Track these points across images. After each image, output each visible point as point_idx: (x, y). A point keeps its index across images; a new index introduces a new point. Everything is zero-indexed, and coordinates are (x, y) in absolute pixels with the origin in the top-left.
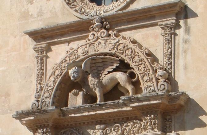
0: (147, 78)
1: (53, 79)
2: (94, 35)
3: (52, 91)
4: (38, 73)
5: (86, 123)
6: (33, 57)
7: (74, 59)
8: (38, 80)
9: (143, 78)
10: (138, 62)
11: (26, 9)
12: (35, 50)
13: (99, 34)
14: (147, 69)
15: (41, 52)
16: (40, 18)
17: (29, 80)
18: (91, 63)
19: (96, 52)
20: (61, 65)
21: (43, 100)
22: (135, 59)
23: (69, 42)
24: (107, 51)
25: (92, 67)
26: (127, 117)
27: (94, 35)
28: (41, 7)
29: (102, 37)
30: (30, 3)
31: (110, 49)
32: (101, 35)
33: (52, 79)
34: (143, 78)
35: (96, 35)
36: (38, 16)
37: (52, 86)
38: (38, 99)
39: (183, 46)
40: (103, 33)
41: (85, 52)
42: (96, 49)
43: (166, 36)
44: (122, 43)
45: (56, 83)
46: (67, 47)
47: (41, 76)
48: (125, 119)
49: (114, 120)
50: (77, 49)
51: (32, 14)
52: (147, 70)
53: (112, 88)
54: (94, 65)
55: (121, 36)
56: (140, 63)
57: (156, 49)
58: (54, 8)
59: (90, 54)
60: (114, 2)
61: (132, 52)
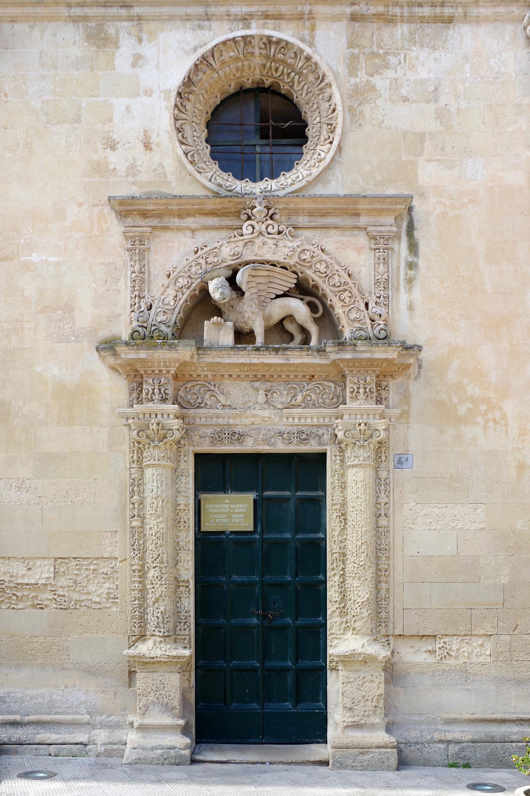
0: (355, 316)
2: (254, 228)
5: (234, 376)
6: (121, 248)
9: (348, 315)
10: (338, 287)
11: (103, 157)
12: (128, 234)
14: (356, 300)
15: (140, 241)
16: (133, 179)
19: (259, 258)
20: (189, 270)
21: (154, 328)
24: (279, 257)
26: (313, 374)
28: (134, 159)
29: (269, 234)
30: (110, 147)
32: (267, 228)
33: (171, 292)
34: (348, 315)
35: (257, 227)
36: (127, 176)
40: (270, 227)
41: (236, 253)
43: (379, 252)
44: (308, 250)
45: (180, 300)
46: (190, 240)
47: (140, 283)
48: (307, 377)
49: (288, 376)
50: (221, 246)
51: (115, 168)
52: (354, 301)
53: (275, 323)
54: (253, 279)
55: (303, 238)
56: (341, 288)
58: (161, 165)
60: (268, 179)
61: (327, 267)
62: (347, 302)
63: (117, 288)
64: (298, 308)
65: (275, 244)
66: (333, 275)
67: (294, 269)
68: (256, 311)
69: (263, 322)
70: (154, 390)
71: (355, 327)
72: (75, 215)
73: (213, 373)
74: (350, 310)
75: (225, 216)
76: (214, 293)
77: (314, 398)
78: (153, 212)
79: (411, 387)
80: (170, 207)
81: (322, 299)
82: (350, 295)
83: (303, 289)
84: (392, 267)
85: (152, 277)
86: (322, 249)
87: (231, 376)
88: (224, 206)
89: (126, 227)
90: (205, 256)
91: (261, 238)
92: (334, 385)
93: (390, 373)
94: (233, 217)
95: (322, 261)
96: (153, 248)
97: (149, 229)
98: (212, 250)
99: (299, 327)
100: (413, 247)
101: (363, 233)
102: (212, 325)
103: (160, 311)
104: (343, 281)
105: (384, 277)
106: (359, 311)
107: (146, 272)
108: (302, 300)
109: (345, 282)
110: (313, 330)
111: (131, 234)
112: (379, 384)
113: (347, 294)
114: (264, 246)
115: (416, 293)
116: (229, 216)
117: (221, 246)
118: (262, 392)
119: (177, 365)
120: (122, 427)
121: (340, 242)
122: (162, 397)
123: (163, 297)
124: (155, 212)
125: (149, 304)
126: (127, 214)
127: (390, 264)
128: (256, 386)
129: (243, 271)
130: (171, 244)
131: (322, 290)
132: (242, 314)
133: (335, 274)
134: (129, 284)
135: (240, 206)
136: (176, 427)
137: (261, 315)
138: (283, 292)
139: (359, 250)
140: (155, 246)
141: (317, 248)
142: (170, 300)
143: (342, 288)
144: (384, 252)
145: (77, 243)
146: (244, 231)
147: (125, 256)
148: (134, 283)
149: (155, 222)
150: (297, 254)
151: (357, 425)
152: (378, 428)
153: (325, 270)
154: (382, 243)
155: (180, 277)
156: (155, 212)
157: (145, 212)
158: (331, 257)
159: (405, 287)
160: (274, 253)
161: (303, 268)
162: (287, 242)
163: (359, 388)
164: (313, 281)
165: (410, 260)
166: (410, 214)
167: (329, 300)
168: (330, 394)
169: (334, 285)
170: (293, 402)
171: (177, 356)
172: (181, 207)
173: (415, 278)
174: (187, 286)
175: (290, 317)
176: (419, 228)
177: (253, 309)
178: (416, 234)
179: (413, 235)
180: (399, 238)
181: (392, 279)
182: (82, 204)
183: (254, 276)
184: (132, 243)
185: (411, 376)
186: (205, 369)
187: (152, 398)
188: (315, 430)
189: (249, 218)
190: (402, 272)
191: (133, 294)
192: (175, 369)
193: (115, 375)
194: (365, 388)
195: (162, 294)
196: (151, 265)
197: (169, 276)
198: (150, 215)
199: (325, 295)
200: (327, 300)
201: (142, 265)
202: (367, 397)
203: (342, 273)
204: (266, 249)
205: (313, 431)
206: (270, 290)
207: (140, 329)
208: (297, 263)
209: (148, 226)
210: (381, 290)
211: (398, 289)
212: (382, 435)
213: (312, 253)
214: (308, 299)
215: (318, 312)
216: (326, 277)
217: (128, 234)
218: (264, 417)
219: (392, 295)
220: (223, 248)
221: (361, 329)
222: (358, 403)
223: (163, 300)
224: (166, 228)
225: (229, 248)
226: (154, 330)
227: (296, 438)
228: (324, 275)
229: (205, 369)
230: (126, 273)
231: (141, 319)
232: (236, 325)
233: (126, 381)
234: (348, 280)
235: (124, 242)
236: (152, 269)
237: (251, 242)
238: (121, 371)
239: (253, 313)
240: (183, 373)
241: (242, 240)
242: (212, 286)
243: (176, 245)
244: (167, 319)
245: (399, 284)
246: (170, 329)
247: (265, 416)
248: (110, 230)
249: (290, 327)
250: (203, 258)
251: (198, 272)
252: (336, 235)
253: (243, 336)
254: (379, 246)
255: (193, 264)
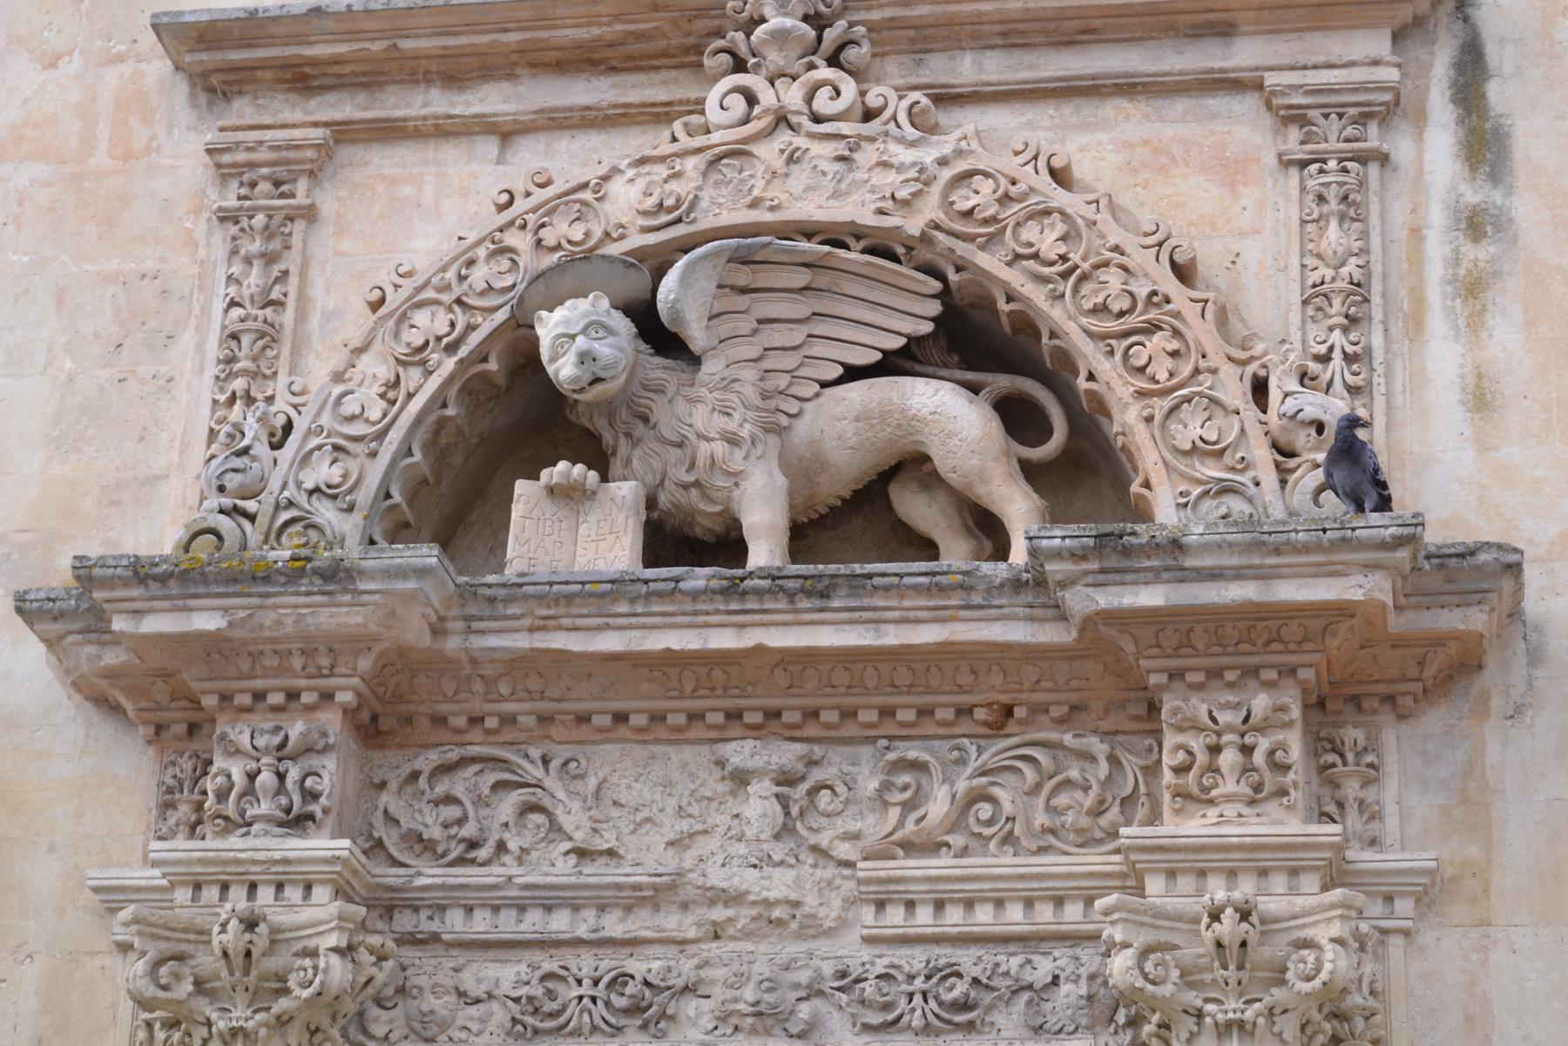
0: (1199, 431)
1: (384, 372)
2: (751, 100)
3: (373, 455)
4: (241, 326)
6: (197, 212)
7: (569, 242)
8: (231, 376)
9: (1163, 426)
10: (1122, 314)
12: (226, 158)
13: (793, 96)
15: (277, 184)
17: (146, 370)
18: (720, 286)
19: (768, 217)
20: (462, 278)
21: (285, 516)
22: (1096, 292)
23: (506, 133)
24: (858, 210)
25: (718, 315)
26: (1005, 699)
27: (751, 100)
29: (817, 119)
31: (889, 204)
32: (809, 99)
33: (375, 367)
35: (767, 97)
37: (375, 414)
38: (239, 503)
39: (1457, 251)
40: (825, 92)
42: (764, 190)
43: (1321, 171)
44: (987, 175)
45: (410, 396)
46: (489, 168)
47: (255, 343)
48: (980, 714)
50: (606, 178)
52: (1197, 371)
53: (847, 494)
56: (1132, 321)
57: (1235, 249)
59: (705, 222)
62: (1162, 376)
63: (164, 369)
64: (950, 417)
65: (841, 159)
66: (1097, 267)
67: (924, 254)
68: (745, 433)
69: (781, 481)
70: (252, 777)
71: (1199, 482)
72: (26, 101)
73: (541, 706)
74: (1175, 409)
75: (641, 69)
76: (553, 359)
77: (1007, 808)
78: (337, 69)
79: (1493, 753)
80: (405, 44)
81: (1057, 372)
82: (1175, 345)
83: (973, 337)
84: (1383, 234)
85: (314, 322)
86: (1053, 173)
87: (621, 718)
88: (631, 27)
89: (222, 130)
90: (531, 219)
91: (784, 137)
92: (1105, 747)
93: (1382, 689)
94: (674, 73)
95: (1047, 212)
96: (328, 204)
97: (317, 134)
98: (567, 193)
99: (959, 510)
100: (1484, 147)
101: (1247, 105)
102: (546, 503)
103: (319, 447)
104: (1142, 292)
105: (1344, 271)
106: (1219, 412)
107: (291, 302)
108: (974, 389)
109: (1154, 293)
110: (1018, 508)
111: (241, 157)
112: (1331, 741)
113: (1160, 342)
114: (793, 167)
115: (1506, 338)
116: (657, 68)
117: (606, 178)
118: (762, 788)
119: (365, 664)
120: (107, 961)
121: (1146, 142)
122: (288, 811)
123: (337, 390)
124: (347, 69)
125: (280, 421)
126: (230, 83)
127: (1374, 220)
128: (735, 760)
129: (689, 268)
130: (407, 191)
131: (1053, 335)
132: (688, 451)
133: (1106, 264)
134: (213, 350)
135: (702, 25)
136: (333, 940)
137: (775, 453)
138: (879, 356)
139: (1232, 172)
140: (340, 199)
141: (1030, 168)
142: (367, 399)
143: (1140, 321)
144: (1345, 170)
145: (20, 203)
146: (713, 113)
147: (208, 245)
148: (233, 344)
149: (346, 107)
150: (936, 189)
151: (1206, 920)
152: (1309, 933)
153: (1062, 249)
154: (1333, 137)
155: (420, 305)
156: (347, 69)
157: (308, 70)
158: (1091, 197)
159: (1449, 311)
160: (836, 195)
161: (961, 248)
162: (893, 147)
163: (1215, 750)
164: (1009, 299)
165: (1472, 196)
166: (1466, 19)
167: (1083, 374)
168: (1086, 789)
169: (1101, 310)
170: (910, 826)
171: (359, 620)
172: (451, 41)
173: (1496, 274)
174: (445, 341)
175: (911, 465)
176: (1508, 68)
177: (732, 425)
178: (1495, 92)
179: (1483, 96)
180: (1419, 118)
181: (1384, 280)
182: (59, 57)
183: (745, 291)
184: (243, 191)
185: (1495, 703)
186: (505, 689)
187: (242, 813)
188: (1015, 962)
189: (740, 66)
190: (1436, 248)
191: (222, 390)
192: (355, 681)
193: (106, 729)
194: (1247, 750)
195: (338, 377)
196: (314, 273)
197: (376, 306)
198: (325, 81)
199: (1066, 360)
200: (1076, 374)
201: (276, 274)
202: (1258, 788)
203: (1140, 258)
204: (800, 178)
205: (1003, 968)
206: (819, 349)
207: (225, 524)
208: (937, 227)
209: (316, 124)
210: (1331, 329)
211: (1416, 324)
212: (1328, 966)
213: (1003, 182)
214: (1003, 382)
215: (1047, 432)
216: (1065, 275)
217: (226, 158)
218: (768, 904)
219: (1387, 351)
220: (616, 187)
221: (1227, 489)
222: (1212, 813)
223: (339, 401)
224: (389, 132)
225: (641, 184)
226: (287, 524)
227: (918, 999)
228: (1059, 268)
229: (505, 689)
230: (206, 311)
231: (232, 481)
232: (663, 499)
233: (151, 751)
234: (1169, 285)
235: (213, 193)
236: (317, 291)
237: (738, 152)
238: (129, 707)
239: (733, 441)
240: (403, 708)
241: (699, 150)
242: (548, 326)
243: (428, 195)
244: (345, 476)
245: (1419, 298)
246: (357, 517)
247: (773, 895)
248: (158, 150)
249: (917, 508)
250: (523, 227)
251: (498, 284)
252: (1128, 117)
253: (687, 540)
254: (1323, 146)
255: (481, 252)
